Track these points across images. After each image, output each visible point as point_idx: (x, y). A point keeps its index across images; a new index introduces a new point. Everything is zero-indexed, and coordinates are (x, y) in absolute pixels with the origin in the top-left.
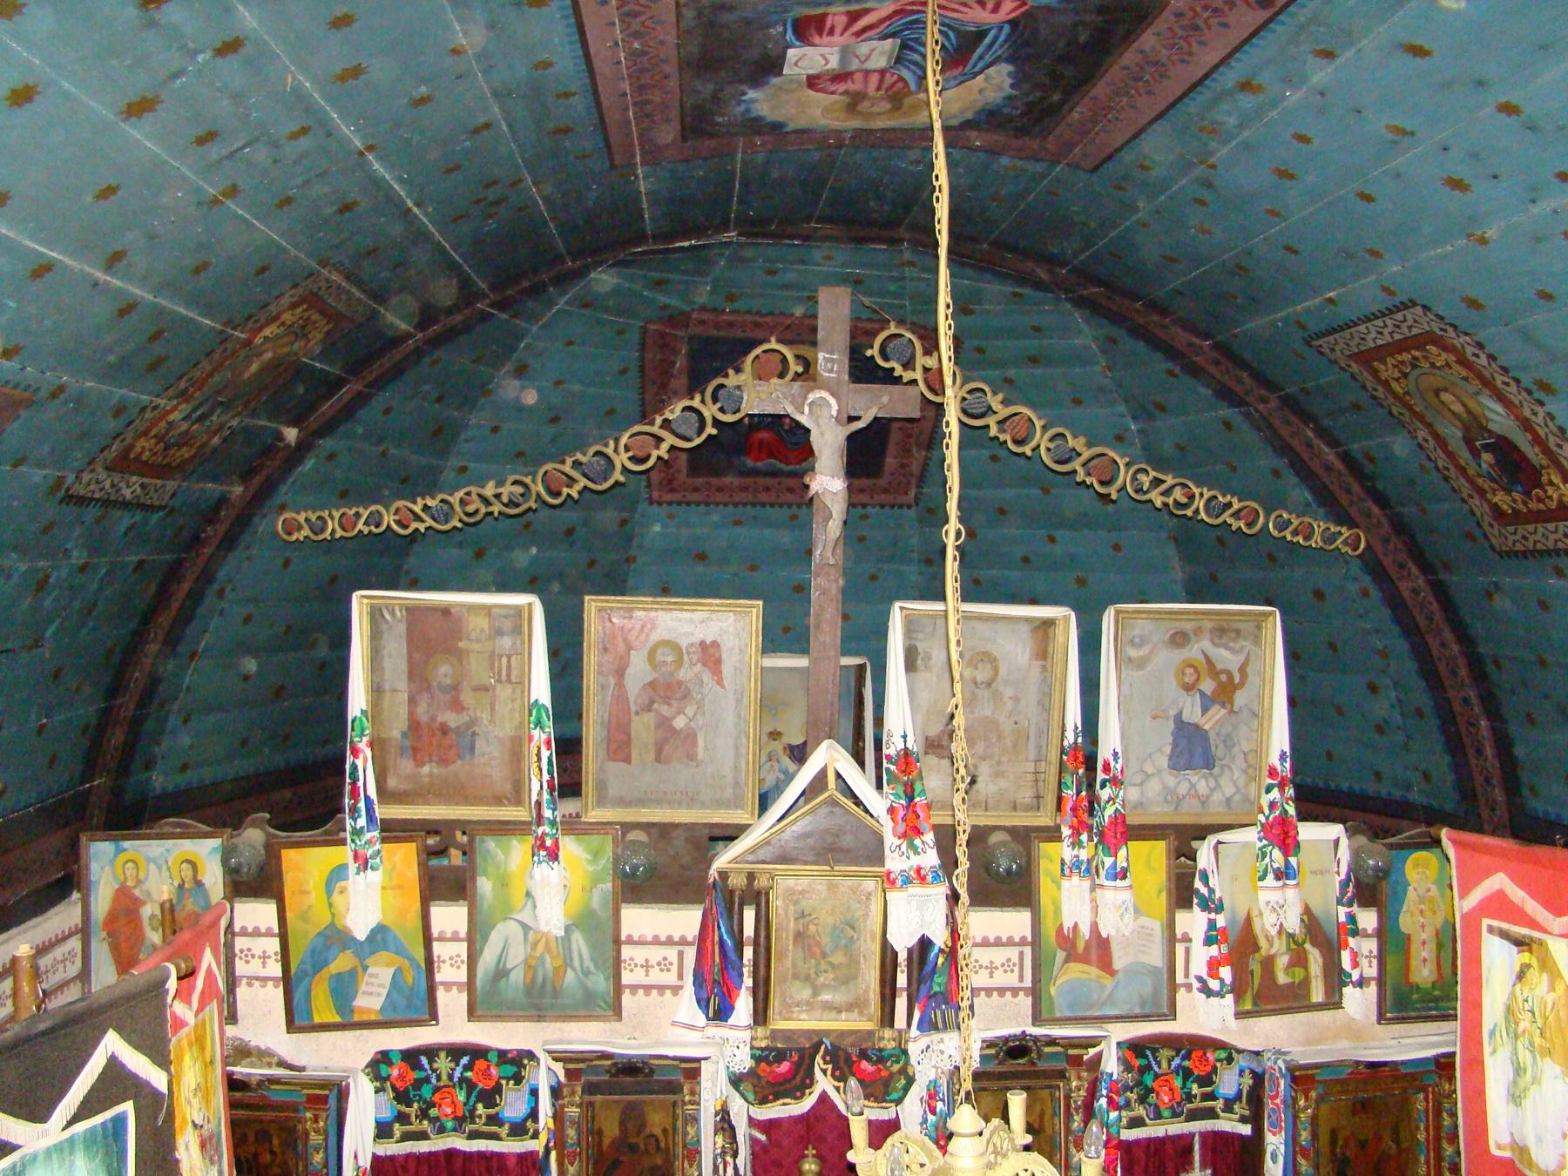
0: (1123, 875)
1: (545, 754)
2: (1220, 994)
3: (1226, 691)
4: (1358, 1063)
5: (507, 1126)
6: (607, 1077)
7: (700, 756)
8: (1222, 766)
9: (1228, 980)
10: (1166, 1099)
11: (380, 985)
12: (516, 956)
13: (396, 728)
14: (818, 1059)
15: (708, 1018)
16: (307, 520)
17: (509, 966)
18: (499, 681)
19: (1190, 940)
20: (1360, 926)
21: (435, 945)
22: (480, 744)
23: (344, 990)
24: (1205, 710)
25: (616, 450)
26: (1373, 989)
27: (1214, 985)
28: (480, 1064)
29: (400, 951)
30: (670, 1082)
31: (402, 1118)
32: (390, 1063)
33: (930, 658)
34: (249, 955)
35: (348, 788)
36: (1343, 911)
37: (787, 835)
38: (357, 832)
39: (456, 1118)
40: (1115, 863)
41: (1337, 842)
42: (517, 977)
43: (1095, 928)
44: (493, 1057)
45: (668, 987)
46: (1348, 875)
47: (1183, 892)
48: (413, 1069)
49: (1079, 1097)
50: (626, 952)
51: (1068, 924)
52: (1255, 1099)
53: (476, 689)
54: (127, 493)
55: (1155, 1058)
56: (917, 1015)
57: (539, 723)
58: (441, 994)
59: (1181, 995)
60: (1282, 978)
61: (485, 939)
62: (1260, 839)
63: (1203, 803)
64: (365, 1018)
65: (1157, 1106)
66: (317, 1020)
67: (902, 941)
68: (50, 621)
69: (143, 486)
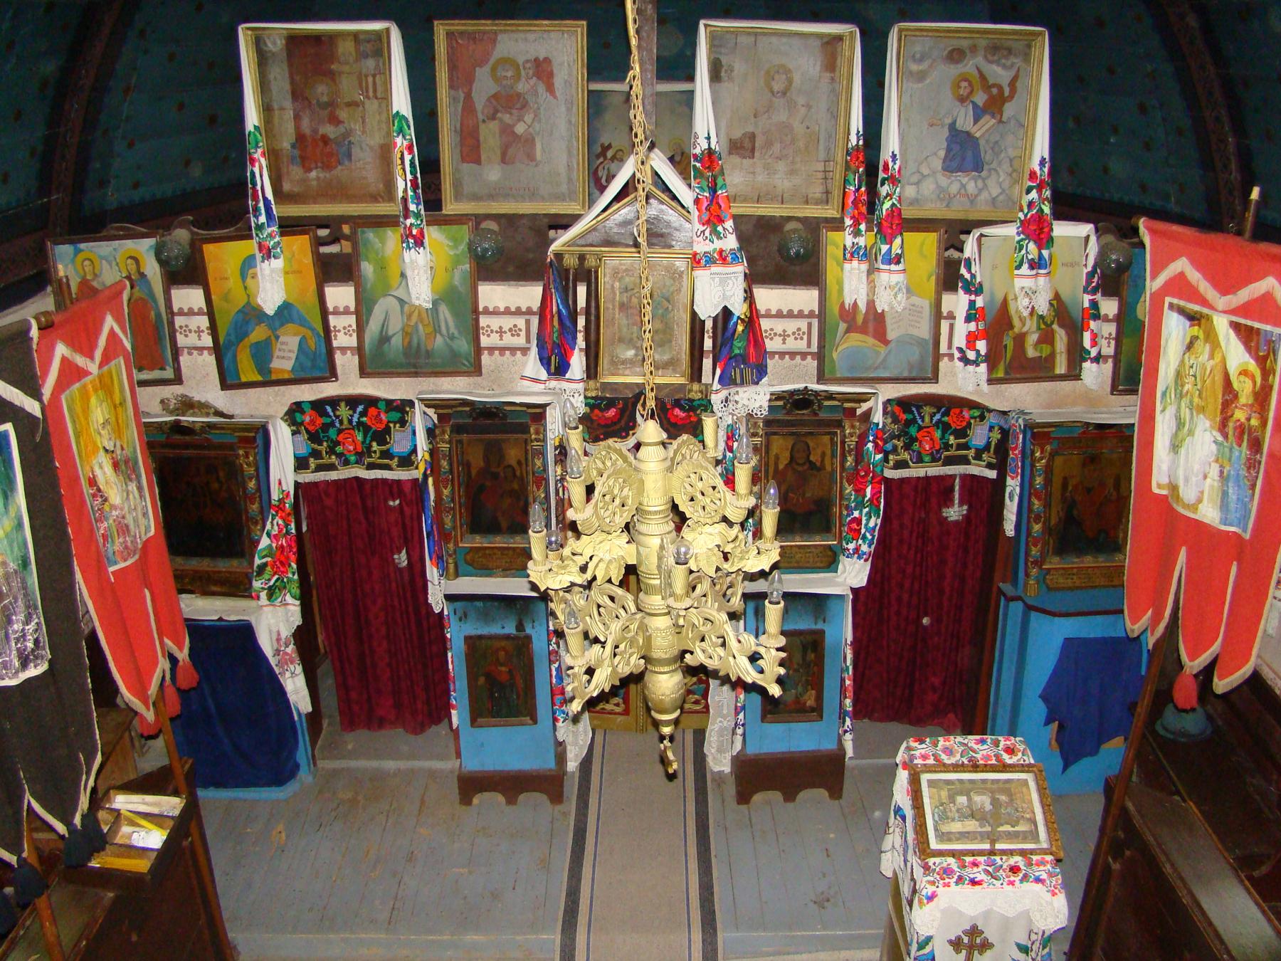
0: (897, 260)
2: (976, 363)
3: (996, 103)
4: (1088, 424)
7: (539, 156)
8: (990, 170)
9: (983, 352)
10: (927, 447)
12: (395, 326)
13: (286, 143)
15: (549, 373)
17: (390, 333)
18: (368, 97)
19: (954, 318)
20: (1103, 312)
21: (331, 317)
23: (262, 354)
24: (976, 121)
26: (1110, 364)
27: (971, 355)
28: (372, 411)
29: (303, 322)
30: (521, 424)
31: (316, 454)
32: (303, 412)
33: (732, 71)
34: (187, 331)
35: (250, 192)
36: (1087, 298)
37: (609, 223)
38: (260, 227)
39: (357, 453)
40: (890, 249)
41: (1087, 238)
42: (397, 342)
43: (871, 304)
44: (382, 405)
45: (519, 349)
46: (1094, 268)
47: (950, 277)
48: (321, 416)
49: (852, 442)
50: (483, 321)
51: (848, 301)
52: (1002, 450)
53: (349, 105)
55: (920, 414)
56: (718, 371)
57: (401, 131)
58: (338, 357)
59: (944, 364)
60: (1031, 353)
61: (370, 312)
62: (1018, 234)
63: (972, 202)
64: (280, 377)
65: (919, 453)
66: (244, 379)
67: (707, 310)
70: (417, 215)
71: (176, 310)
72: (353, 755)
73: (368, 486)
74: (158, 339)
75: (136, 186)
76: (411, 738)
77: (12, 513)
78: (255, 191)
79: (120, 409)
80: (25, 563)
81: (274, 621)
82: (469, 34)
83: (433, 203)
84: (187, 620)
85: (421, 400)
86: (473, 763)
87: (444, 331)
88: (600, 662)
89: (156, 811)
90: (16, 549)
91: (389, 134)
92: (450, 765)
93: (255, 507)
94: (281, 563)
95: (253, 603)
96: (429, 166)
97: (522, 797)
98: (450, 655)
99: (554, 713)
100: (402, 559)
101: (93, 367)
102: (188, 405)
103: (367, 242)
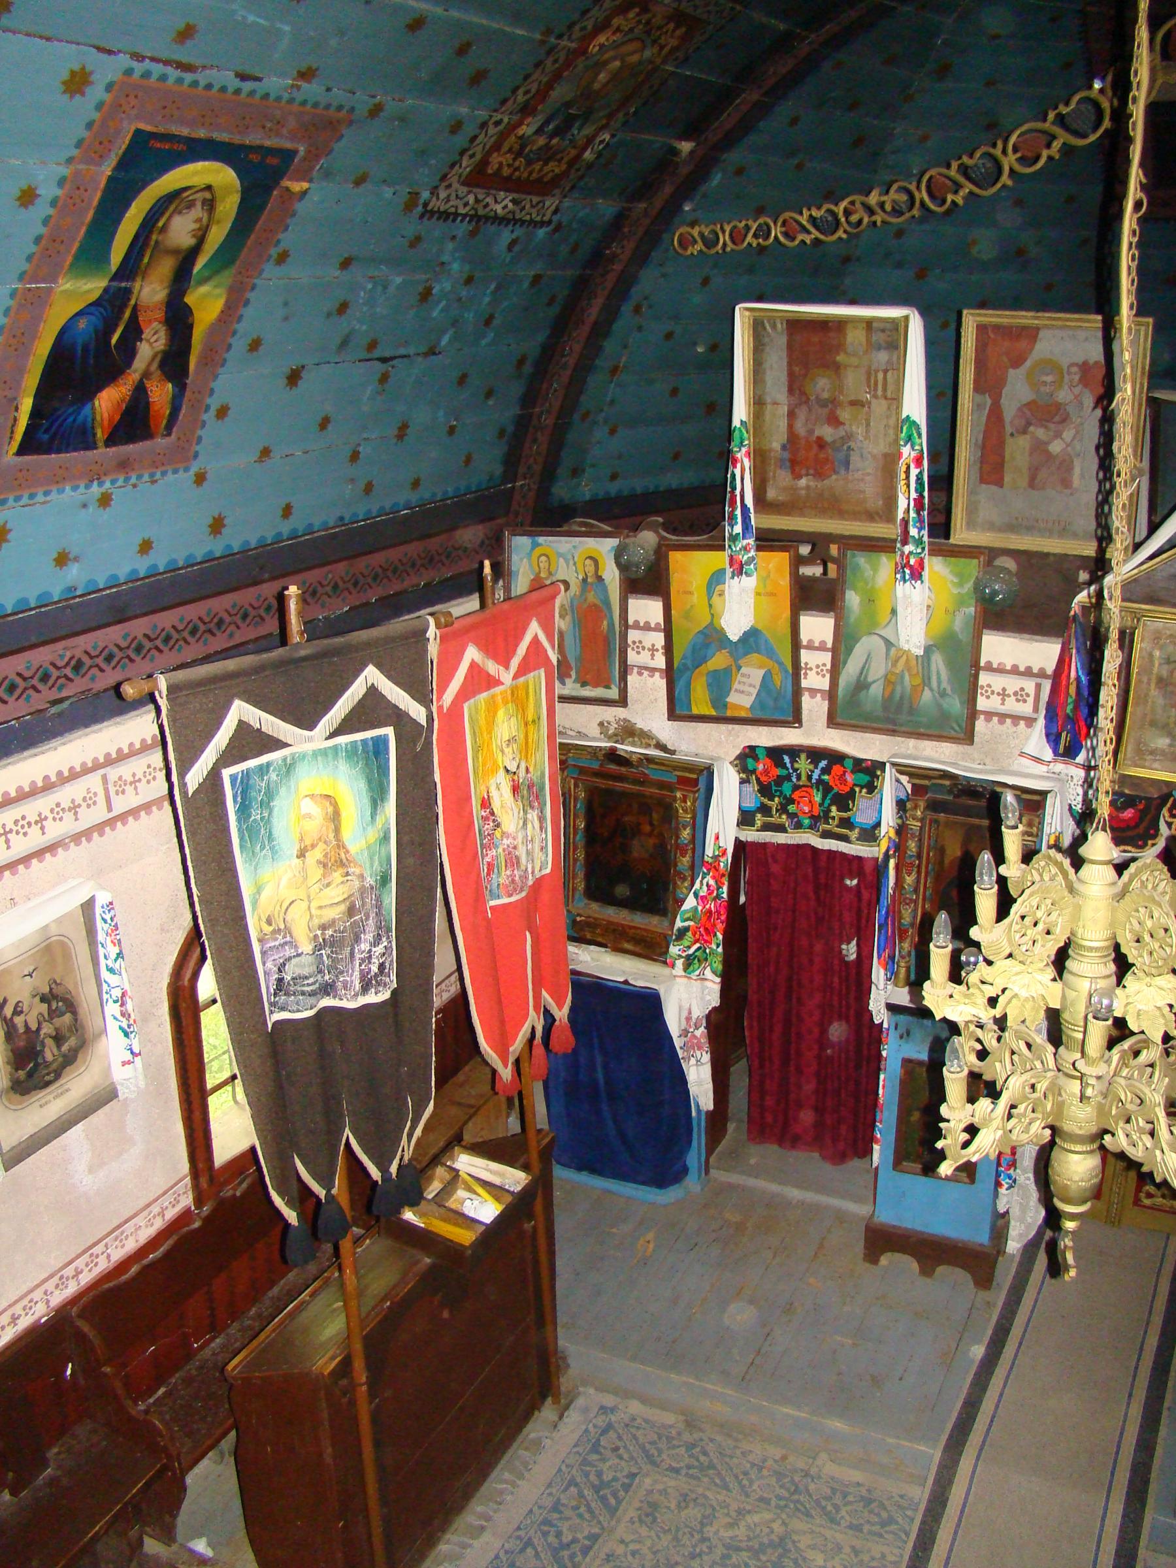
1: (914, 472)
5: (857, 831)
6: (951, 798)
11: (750, 685)
12: (877, 671)
13: (776, 442)
14: (1165, 811)
15: (1056, 753)
16: (701, 234)
17: (870, 680)
18: (875, 397)
21: (803, 652)
22: (855, 458)
23: (720, 684)
25: (1004, 152)
28: (837, 769)
29: (771, 654)
31: (765, 810)
32: (756, 758)
34: (640, 647)
38: (734, 538)
39: (812, 817)
42: (876, 690)
44: (849, 764)
48: (777, 766)
50: (984, 678)
53: (853, 403)
54: (499, 208)
58: (806, 699)
61: (849, 651)
64: (736, 714)
68: (444, 332)
69: (514, 201)
70: (919, 542)
71: (630, 622)
72: (755, 1172)
73: (824, 858)
74: (607, 653)
75: (614, 477)
76: (828, 1167)
77: (380, 820)
78: (733, 497)
79: (531, 728)
80: (384, 880)
81: (688, 995)
82: (1004, 327)
83: (940, 527)
84: (574, 972)
85: (894, 764)
86: (886, 1216)
87: (934, 684)
88: (987, 1120)
89: (497, 1180)
90: (376, 863)
91: (896, 440)
92: (864, 1210)
93: (686, 860)
94: (706, 929)
95: (667, 971)
96: (942, 481)
97: (940, 1269)
98: (882, 1077)
99: (998, 1175)
100: (850, 951)
101: (507, 677)
102: (629, 731)
103: (857, 568)
